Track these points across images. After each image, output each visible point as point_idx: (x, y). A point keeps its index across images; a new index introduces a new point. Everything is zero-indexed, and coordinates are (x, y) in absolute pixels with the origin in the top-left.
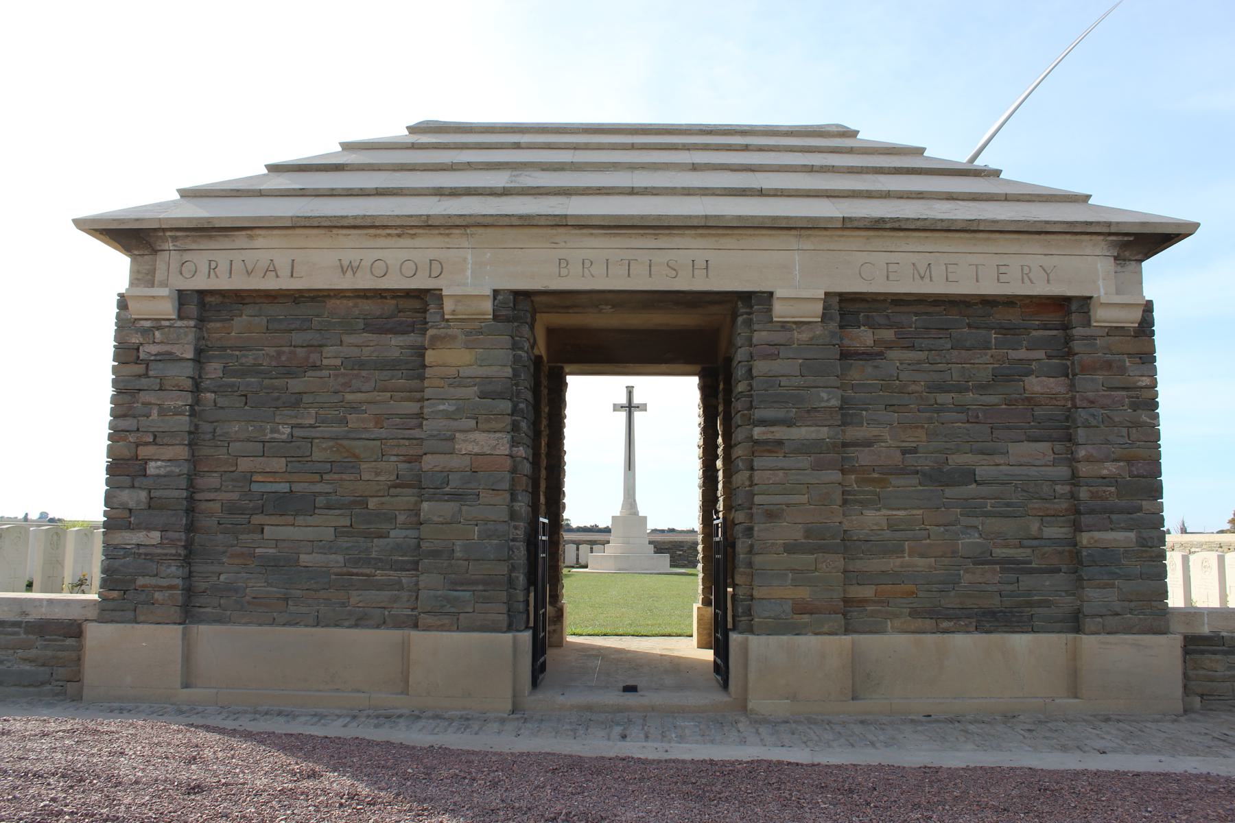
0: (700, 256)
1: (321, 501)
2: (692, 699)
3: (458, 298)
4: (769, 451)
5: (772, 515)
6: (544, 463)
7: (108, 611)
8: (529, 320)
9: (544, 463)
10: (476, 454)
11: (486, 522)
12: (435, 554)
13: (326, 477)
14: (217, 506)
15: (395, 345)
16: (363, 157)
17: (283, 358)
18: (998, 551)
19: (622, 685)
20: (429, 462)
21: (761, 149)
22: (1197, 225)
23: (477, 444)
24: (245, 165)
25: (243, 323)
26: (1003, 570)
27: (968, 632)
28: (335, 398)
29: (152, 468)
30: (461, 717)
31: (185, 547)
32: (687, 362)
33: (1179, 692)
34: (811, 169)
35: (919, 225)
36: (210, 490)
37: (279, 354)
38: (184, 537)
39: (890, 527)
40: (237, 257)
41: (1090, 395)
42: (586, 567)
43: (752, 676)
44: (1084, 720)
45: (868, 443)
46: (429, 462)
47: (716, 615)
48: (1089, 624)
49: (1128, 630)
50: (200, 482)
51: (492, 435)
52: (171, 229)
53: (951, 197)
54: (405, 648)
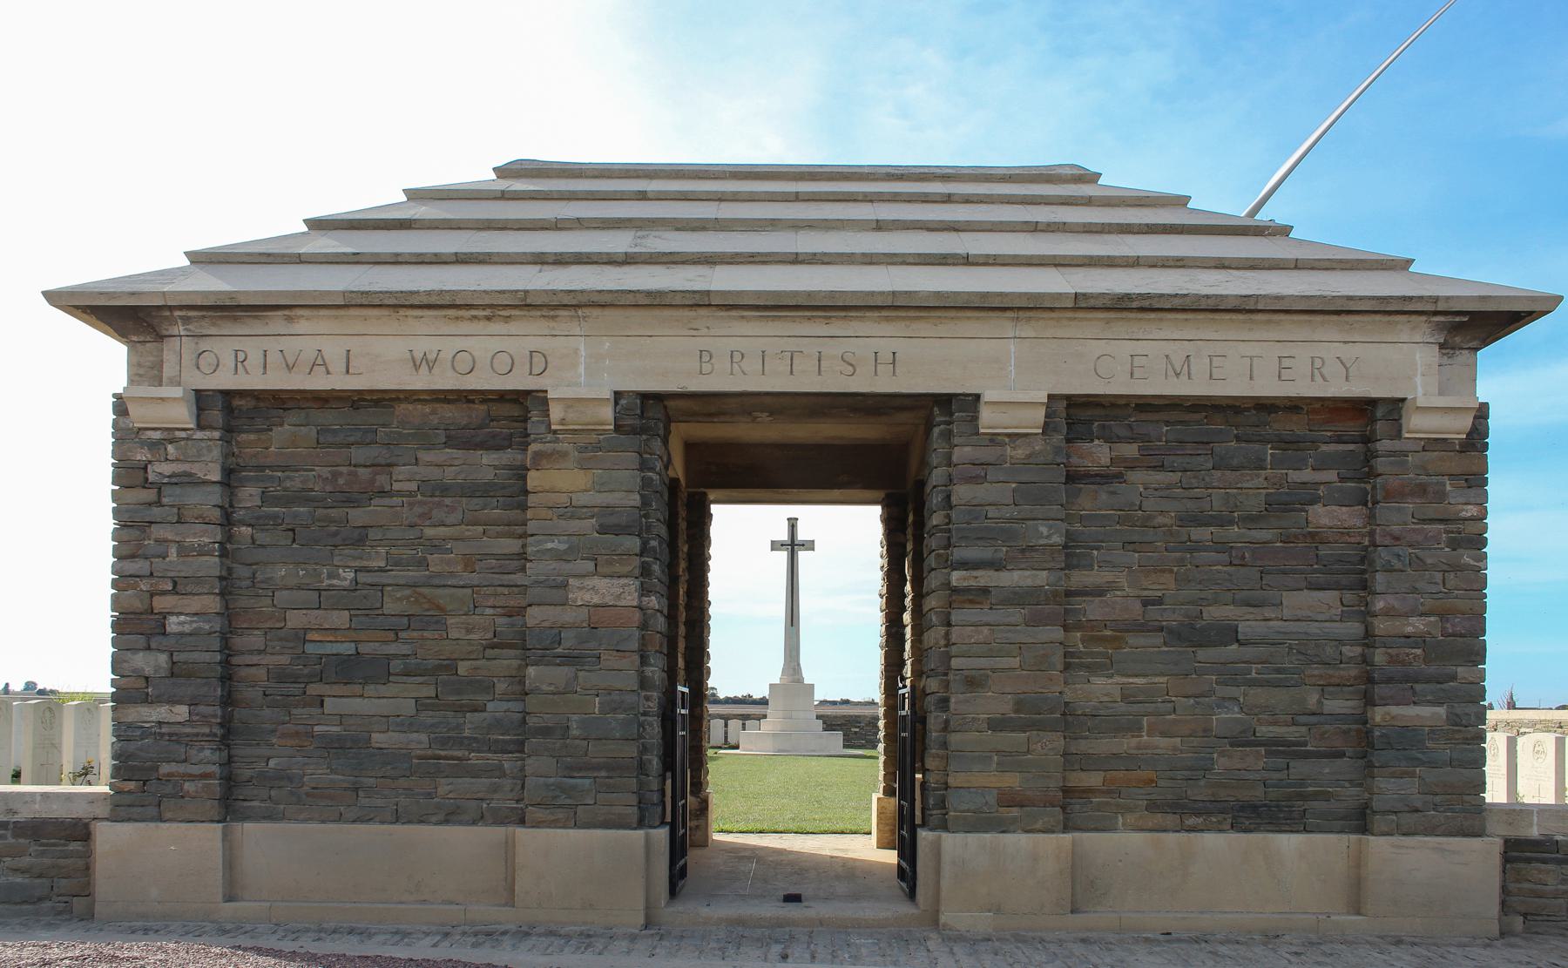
0: (885, 347)
1: (396, 666)
2: (869, 911)
3: (569, 403)
4: (971, 602)
5: (973, 683)
6: (682, 617)
7: (122, 808)
8: (661, 432)
9: (682, 617)
10: (596, 606)
11: (609, 691)
12: (545, 732)
13: (402, 635)
14: (261, 673)
15: (487, 464)
16: (435, 210)
17: (341, 481)
18: (1264, 728)
19: (782, 894)
20: (535, 616)
21: (968, 200)
22: (1560, 298)
23: (597, 592)
24: (276, 217)
25: (284, 436)
26: (1269, 754)
27: (1220, 831)
28: (412, 534)
29: (173, 624)
30: (581, 934)
31: (221, 725)
32: (867, 487)
33: (1495, 909)
34: (1034, 228)
35: (1177, 303)
36: (251, 652)
37: (335, 475)
38: (219, 713)
39: (1124, 698)
40: (273, 345)
41: (1395, 529)
42: (737, 747)
43: (945, 883)
44: (1367, 942)
45: (1099, 592)
46: (535, 616)
47: (901, 807)
48: (1378, 822)
49: (1431, 831)
50: (238, 642)
51: (615, 581)
52: (181, 308)
53: (1221, 264)
54: (509, 847)
